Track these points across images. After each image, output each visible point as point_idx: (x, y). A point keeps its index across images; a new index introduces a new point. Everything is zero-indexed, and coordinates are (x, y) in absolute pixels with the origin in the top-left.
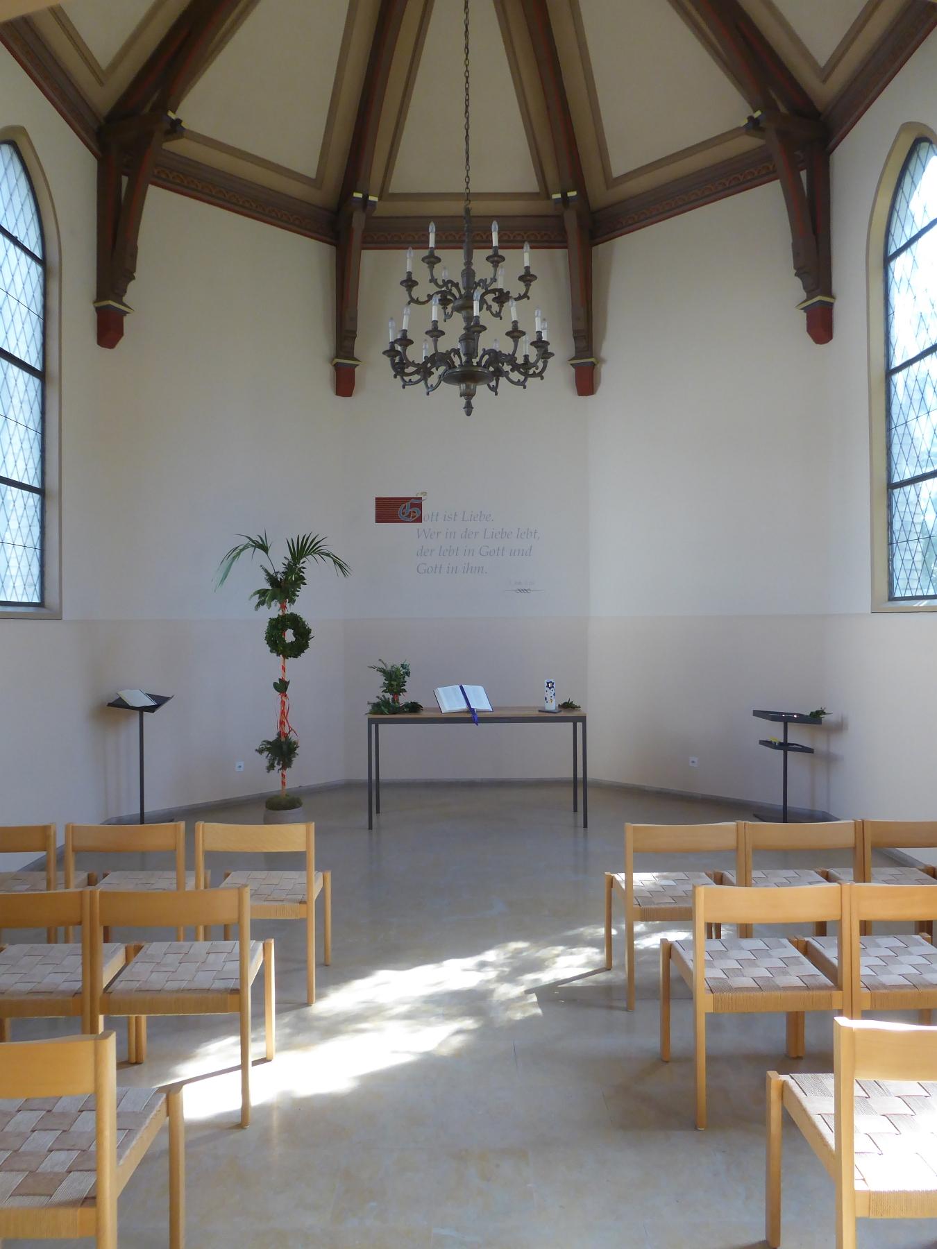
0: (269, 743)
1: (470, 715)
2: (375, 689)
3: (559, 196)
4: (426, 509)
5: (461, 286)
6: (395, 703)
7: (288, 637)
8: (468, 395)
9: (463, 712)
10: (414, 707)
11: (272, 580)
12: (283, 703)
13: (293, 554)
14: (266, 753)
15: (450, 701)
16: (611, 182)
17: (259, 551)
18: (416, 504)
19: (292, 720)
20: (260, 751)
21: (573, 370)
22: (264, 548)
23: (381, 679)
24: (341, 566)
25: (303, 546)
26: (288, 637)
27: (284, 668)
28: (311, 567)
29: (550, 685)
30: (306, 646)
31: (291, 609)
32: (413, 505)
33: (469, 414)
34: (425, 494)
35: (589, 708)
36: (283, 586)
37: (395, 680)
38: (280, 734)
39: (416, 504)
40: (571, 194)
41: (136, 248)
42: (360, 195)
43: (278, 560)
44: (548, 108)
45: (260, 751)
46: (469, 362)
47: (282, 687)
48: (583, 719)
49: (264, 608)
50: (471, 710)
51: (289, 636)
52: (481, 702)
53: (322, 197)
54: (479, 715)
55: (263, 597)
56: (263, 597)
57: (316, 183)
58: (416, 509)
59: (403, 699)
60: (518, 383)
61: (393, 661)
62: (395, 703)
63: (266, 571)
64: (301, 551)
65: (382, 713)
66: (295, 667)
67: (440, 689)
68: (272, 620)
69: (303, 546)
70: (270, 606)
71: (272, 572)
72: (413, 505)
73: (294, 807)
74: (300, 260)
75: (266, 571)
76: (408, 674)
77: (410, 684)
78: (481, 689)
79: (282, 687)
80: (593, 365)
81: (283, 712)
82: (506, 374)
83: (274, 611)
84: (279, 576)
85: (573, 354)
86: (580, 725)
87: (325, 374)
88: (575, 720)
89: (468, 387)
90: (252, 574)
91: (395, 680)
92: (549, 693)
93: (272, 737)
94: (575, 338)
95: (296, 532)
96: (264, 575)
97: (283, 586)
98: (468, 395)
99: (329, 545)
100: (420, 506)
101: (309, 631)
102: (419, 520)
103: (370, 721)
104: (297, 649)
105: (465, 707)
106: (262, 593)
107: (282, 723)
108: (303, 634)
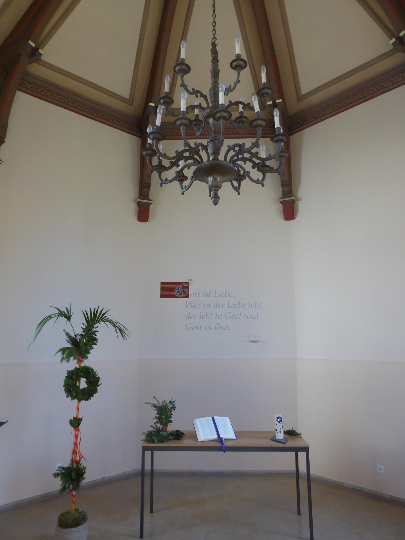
0: (63, 468)
1: (219, 445)
2: (149, 420)
3: (271, 103)
4: (192, 289)
5: (208, 98)
6: (164, 433)
7: (82, 384)
8: (214, 189)
9: (214, 440)
10: (178, 435)
11: (73, 341)
12: (76, 436)
13: (87, 321)
14: (59, 478)
15: (205, 432)
16: (300, 98)
17: (63, 319)
18: (186, 286)
19: (83, 449)
20: (56, 475)
21: (281, 206)
22: (68, 318)
23: (154, 413)
24: (121, 330)
25: (95, 315)
26: (82, 384)
27: (78, 409)
28: (102, 331)
29: (279, 420)
30: (95, 391)
31: (86, 363)
32: (183, 287)
33: (216, 203)
34: (191, 280)
35: (308, 437)
36: (80, 346)
37: (164, 413)
38: (73, 461)
39: (186, 286)
40: (278, 101)
41: (7, 124)
42: (153, 105)
43: (77, 327)
44: (264, 52)
45: (56, 475)
46: (216, 159)
47: (76, 423)
48: (306, 449)
49: (65, 362)
50: (220, 440)
51: (83, 384)
52: (228, 433)
53: (130, 110)
54: (227, 444)
55: (67, 353)
56: (67, 353)
57: (130, 101)
58: (185, 290)
59: (171, 428)
60: (257, 182)
61: (164, 398)
62: (164, 433)
63: (67, 334)
64: (94, 318)
65: (153, 441)
66: (87, 409)
67: (197, 420)
68: (69, 372)
69: (95, 315)
70: (68, 361)
71: (73, 335)
72: (183, 287)
73: (78, 524)
74: (119, 146)
75: (67, 334)
76: (174, 408)
77: (175, 416)
78: (227, 420)
79: (76, 423)
80: (294, 201)
81: (76, 444)
82: (247, 174)
83: (73, 364)
84: (78, 337)
85: (281, 196)
86: (302, 455)
87: (132, 209)
88: (296, 450)
89: (215, 179)
90: (57, 335)
91: (164, 413)
92: (279, 426)
93: (67, 463)
94: (282, 186)
95: (89, 306)
96: (66, 337)
97: (80, 346)
98: (214, 189)
99: (112, 315)
100: (188, 288)
101: (98, 379)
102: (187, 296)
103: (144, 449)
104: (88, 394)
105: (215, 436)
106: (63, 350)
107: (74, 452)
108: (94, 381)
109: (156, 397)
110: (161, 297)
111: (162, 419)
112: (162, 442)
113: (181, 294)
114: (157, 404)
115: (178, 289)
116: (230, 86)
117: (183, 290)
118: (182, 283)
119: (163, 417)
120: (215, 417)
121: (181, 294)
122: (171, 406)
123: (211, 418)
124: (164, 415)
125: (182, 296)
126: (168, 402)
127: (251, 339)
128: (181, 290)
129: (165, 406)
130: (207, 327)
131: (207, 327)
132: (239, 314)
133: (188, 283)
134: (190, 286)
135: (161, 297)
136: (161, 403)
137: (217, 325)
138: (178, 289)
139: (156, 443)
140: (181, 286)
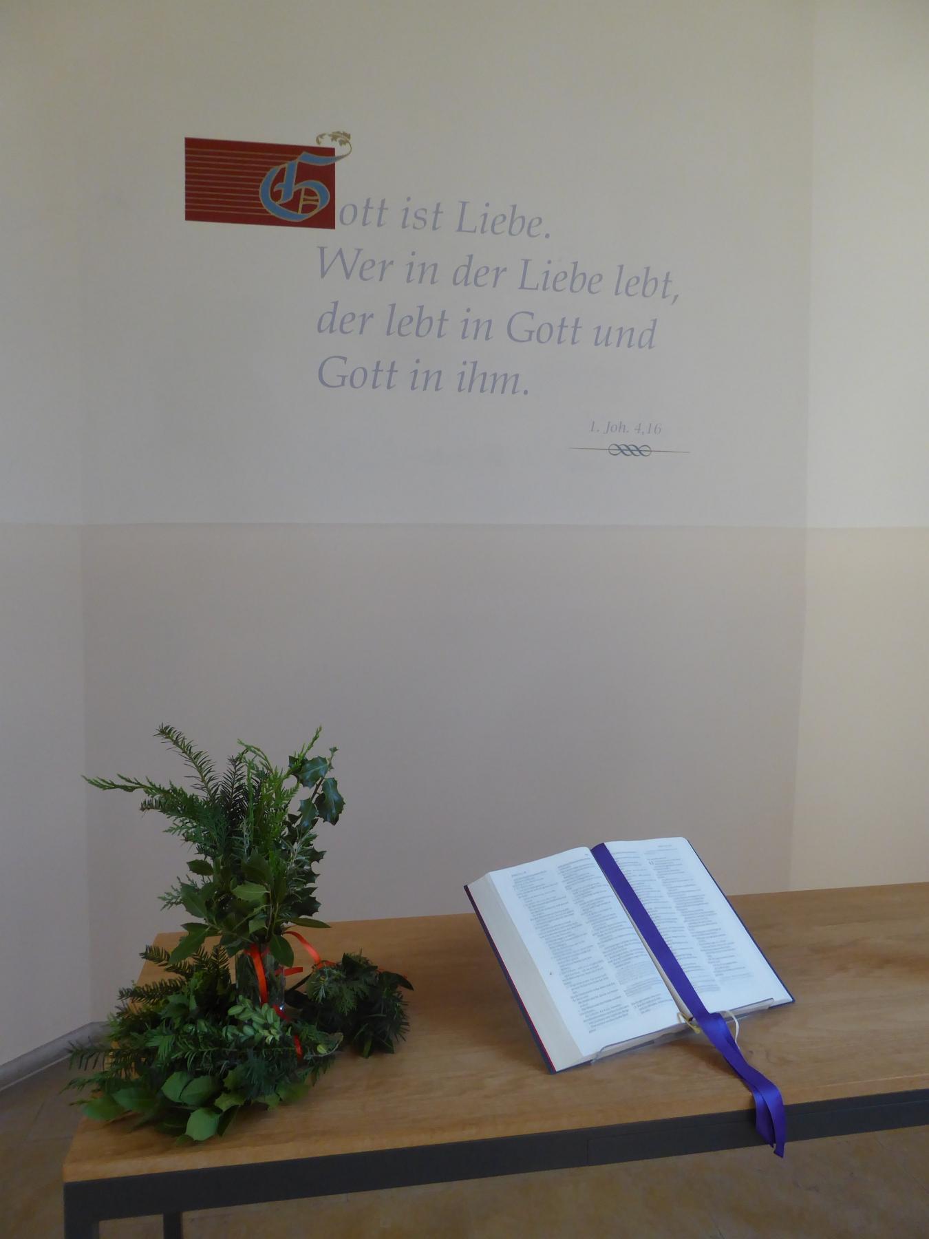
15: (589, 998)
23: (173, 855)
32: (305, 172)
34: (345, 138)
54: (795, 1089)
58: (315, 185)
65: (169, 1122)
72: (305, 172)
76: (327, 807)
100: (327, 176)
102: (325, 219)
105: (667, 1014)
109: (178, 727)
110: (190, 216)
111: (245, 910)
112: (242, 1114)
113: (293, 205)
114: (190, 785)
115: (280, 178)
116: (146, 807)
117: (303, 186)
118: (294, 150)
119: (252, 893)
120: (616, 848)
121: (293, 205)
122: (305, 793)
123: (583, 854)
124: (255, 876)
125: (300, 215)
126: (281, 765)
127: (622, 439)
128: (290, 187)
129: (252, 794)
130: (421, 379)
131: (421, 379)
132: (570, 322)
133: (330, 152)
134: (339, 167)
135: (190, 216)
136: (221, 770)
137: (468, 369)
138: (280, 178)
139: (193, 1144)
140: (291, 167)
